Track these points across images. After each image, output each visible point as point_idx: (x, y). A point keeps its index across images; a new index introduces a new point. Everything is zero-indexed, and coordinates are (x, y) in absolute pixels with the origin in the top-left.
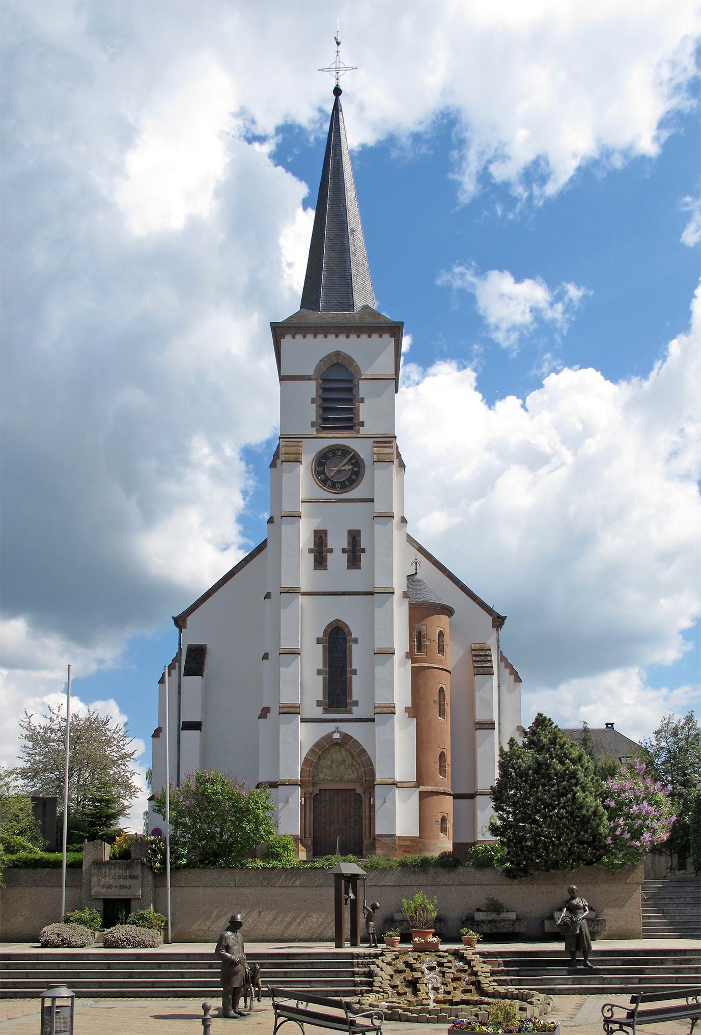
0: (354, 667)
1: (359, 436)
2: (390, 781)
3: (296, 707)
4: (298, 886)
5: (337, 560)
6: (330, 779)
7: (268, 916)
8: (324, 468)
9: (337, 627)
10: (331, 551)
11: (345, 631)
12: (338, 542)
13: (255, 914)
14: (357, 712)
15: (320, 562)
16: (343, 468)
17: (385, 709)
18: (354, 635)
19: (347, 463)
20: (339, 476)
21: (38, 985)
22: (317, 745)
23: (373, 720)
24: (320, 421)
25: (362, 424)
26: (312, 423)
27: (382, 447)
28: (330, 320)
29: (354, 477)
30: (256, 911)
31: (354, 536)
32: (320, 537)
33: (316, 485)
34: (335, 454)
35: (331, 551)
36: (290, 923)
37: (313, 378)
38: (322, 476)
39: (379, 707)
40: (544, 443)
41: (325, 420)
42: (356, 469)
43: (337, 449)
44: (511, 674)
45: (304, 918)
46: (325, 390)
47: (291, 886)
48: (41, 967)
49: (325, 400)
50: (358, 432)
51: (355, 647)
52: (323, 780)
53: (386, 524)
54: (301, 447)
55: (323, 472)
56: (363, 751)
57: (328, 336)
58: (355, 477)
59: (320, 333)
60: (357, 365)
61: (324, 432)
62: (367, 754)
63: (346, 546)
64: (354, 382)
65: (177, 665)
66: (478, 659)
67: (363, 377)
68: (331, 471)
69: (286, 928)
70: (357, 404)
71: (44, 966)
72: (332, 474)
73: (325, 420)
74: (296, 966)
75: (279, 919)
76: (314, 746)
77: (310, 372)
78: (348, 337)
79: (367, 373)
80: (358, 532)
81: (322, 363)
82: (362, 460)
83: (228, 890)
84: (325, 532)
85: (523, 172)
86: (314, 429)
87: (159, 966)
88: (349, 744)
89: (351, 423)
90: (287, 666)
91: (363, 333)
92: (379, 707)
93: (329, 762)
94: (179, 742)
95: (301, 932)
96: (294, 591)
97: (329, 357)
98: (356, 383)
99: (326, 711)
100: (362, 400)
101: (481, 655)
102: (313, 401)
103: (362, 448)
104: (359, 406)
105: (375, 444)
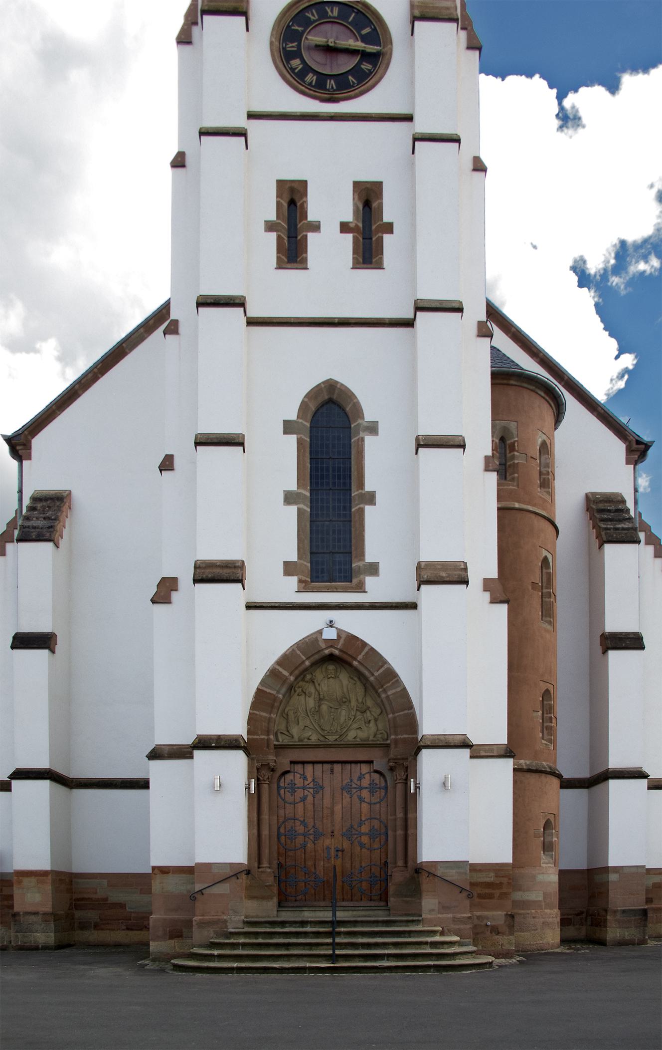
10: (316, 227)
34: (323, 15)
35: (345, 228)
63: (349, 217)
93: (311, 703)
99: (304, 587)
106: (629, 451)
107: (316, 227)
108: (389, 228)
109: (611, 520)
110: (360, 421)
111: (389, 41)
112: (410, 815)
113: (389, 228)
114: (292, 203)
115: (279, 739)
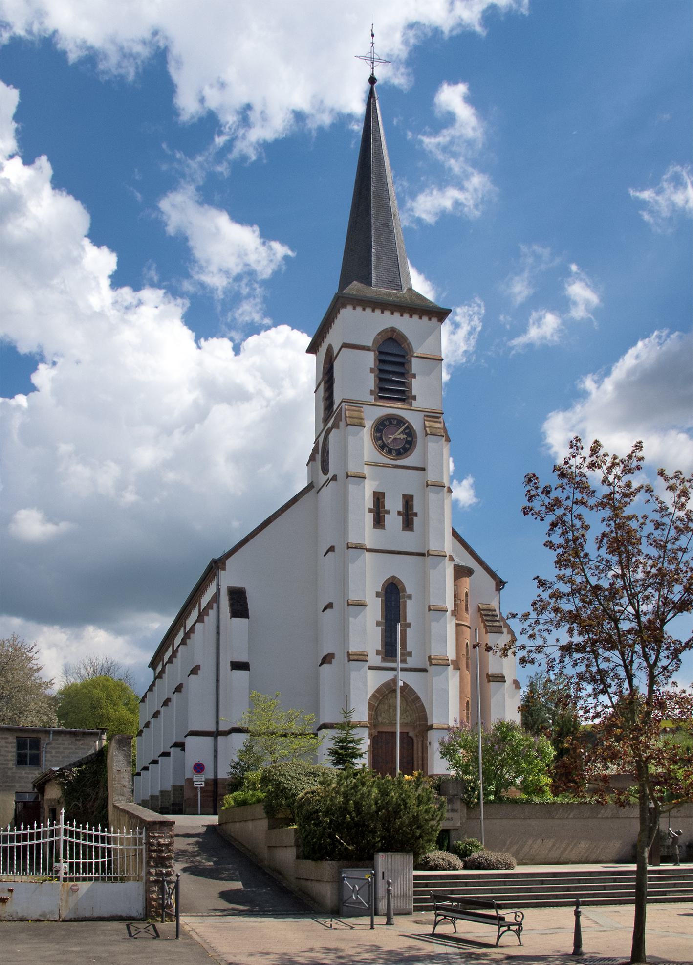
0: (408, 621)
1: (412, 408)
2: (446, 726)
3: (365, 655)
4: (571, 818)
5: (394, 520)
6: (387, 722)
7: (549, 843)
8: (382, 434)
9: (392, 583)
10: (388, 512)
11: (399, 587)
12: (394, 504)
13: (539, 841)
14: (411, 662)
15: (379, 522)
16: (398, 437)
17: (440, 661)
18: (409, 591)
19: (402, 432)
20: (395, 444)
21: (511, 898)
22: (378, 691)
23: (425, 670)
24: (377, 390)
25: (414, 398)
26: (371, 391)
27: (434, 422)
28: (385, 297)
29: (407, 446)
30: (540, 839)
31: (408, 501)
32: (379, 498)
33: (374, 448)
34: (391, 423)
35: (399, 513)
36: (565, 849)
37: (371, 348)
38: (380, 442)
39: (436, 659)
40: (250, 383)
41: (382, 390)
42: (409, 439)
43: (393, 418)
44: (508, 633)
45: (575, 844)
46: (381, 361)
47: (567, 818)
48: (492, 884)
49: (381, 371)
50: (411, 405)
51: (409, 603)
52: (381, 723)
53: (359, 484)
54: (363, 412)
55: (380, 438)
56: (418, 698)
57: (423, 318)
58: (408, 446)
59: (378, 308)
60: (410, 343)
61: (380, 400)
62: (421, 701)
63: (401, 509)
64: (406, 357)
65: (215, 605)
66: (488, 618)
67: (415, 355)
68: (389, 438)
69: (562, 853)
70: (410, 379)
71: (486, 884)
72: (389, 441)
73: (382, 390)
74: (673, 879)
75: (557, 845)
76: (376, 691)
77: (370, 343)
78: (402, 315)
79: (418, 351)
80: (412, 497)
81: (380, 336)
82: (415, 431)
83: (519, 822)
84: (383, 494)
85: (481, 174)
86: (373, 397)
87: (579, 881)
88: (406, 691)
89: (404, 396)
90: (355, 617)
91: (415, 313)
92: (436, 659)
93: (386, 707)
94: (218, 681)
95: (573, 856)
96: (360, 547)
97: (385, 331)
98: (409, 359)
99: (384, 660)
100: (414, 376)
101: (489, 615)
102: (372, 370)
103: (415, 420)
104: (411, 381)
105: (425, 418)
106: (497, 585)
107: (388, 512)
108: (416, 515)
109: (490, 621)
110: (405, 593)
111: (416, 437)
112: (425, 755)
113: (416, 515)
114: (378, 499)
115: (157, 665)
